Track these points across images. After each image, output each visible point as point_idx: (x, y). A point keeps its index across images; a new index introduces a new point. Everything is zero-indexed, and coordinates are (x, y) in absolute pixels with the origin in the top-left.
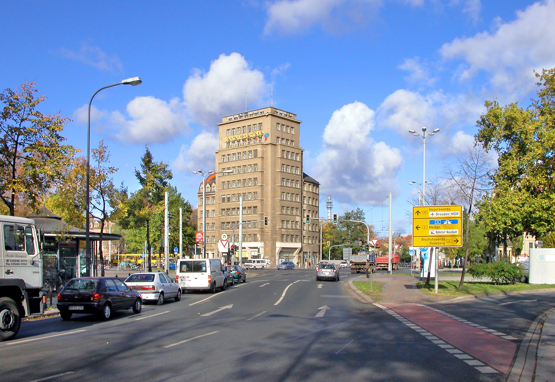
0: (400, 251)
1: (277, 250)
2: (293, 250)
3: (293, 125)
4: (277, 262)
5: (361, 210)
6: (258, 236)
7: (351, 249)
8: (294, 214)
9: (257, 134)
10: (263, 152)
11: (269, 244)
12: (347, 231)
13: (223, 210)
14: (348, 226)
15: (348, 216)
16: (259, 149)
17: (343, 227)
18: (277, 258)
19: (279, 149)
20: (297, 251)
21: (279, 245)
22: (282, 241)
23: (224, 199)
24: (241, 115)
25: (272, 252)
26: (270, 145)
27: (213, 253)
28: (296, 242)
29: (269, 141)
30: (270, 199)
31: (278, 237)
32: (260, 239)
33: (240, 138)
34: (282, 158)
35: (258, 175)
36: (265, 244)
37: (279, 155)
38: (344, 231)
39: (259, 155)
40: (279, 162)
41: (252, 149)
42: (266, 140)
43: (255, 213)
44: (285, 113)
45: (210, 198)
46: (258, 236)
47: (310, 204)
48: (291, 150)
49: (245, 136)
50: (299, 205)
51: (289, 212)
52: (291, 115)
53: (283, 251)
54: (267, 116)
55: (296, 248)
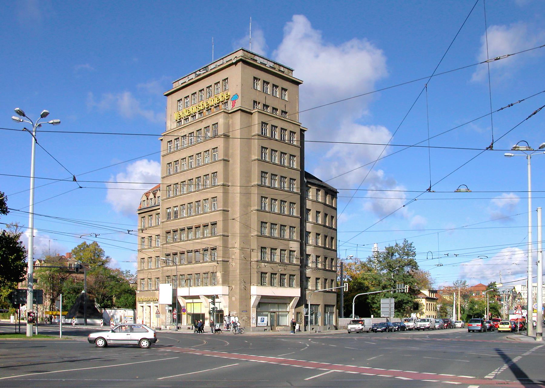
0: (467, 306)
1: (253, 300)
2: (284, 301)
3: (286, 85)
4: (253, 321)
5: (409, 242)
6: (219, 275)
7: (393, 300)
8: (287, 236)
9: (220, 97)
10: (227, 126)
11: (237, 288)
12: (388, 274)
13: (168, 232)
14: (390, 267)
15: (390, 252)
16: (221, 120)
17: (382, 269)
18: (253, 314)
19: (256, 119)
20: (293, 303)
21: (257, 291)
22: (262, 284)
23: (169, 214)
24: (197, 73)
25: (241, 303)
26: (239, 114)
27: (150, 306)
28: (290, 286)
29: (238, 105)
30: (238, 208)
31: (255, 277)
32: (220, 280)
33: (195, 110)
34: (262, 135)
35: (219, 168)
36: (231, 289)
37: (256, 130)
38: (384, 275)
39: (221, 131)
40: (256, 144)
41: (210, 122)
42: (233, 106)
43: (213, 234)
44: (272, 65)
45: (154, 216)
46: (219, 275)
47: (320, 222)
48: (280, 124)
49: (203, 105)
50: (296, 223)
51: (276, 234)
52: (282, 69)
53: (265, 303)
54: (236, 63)
55: (291, 298)
